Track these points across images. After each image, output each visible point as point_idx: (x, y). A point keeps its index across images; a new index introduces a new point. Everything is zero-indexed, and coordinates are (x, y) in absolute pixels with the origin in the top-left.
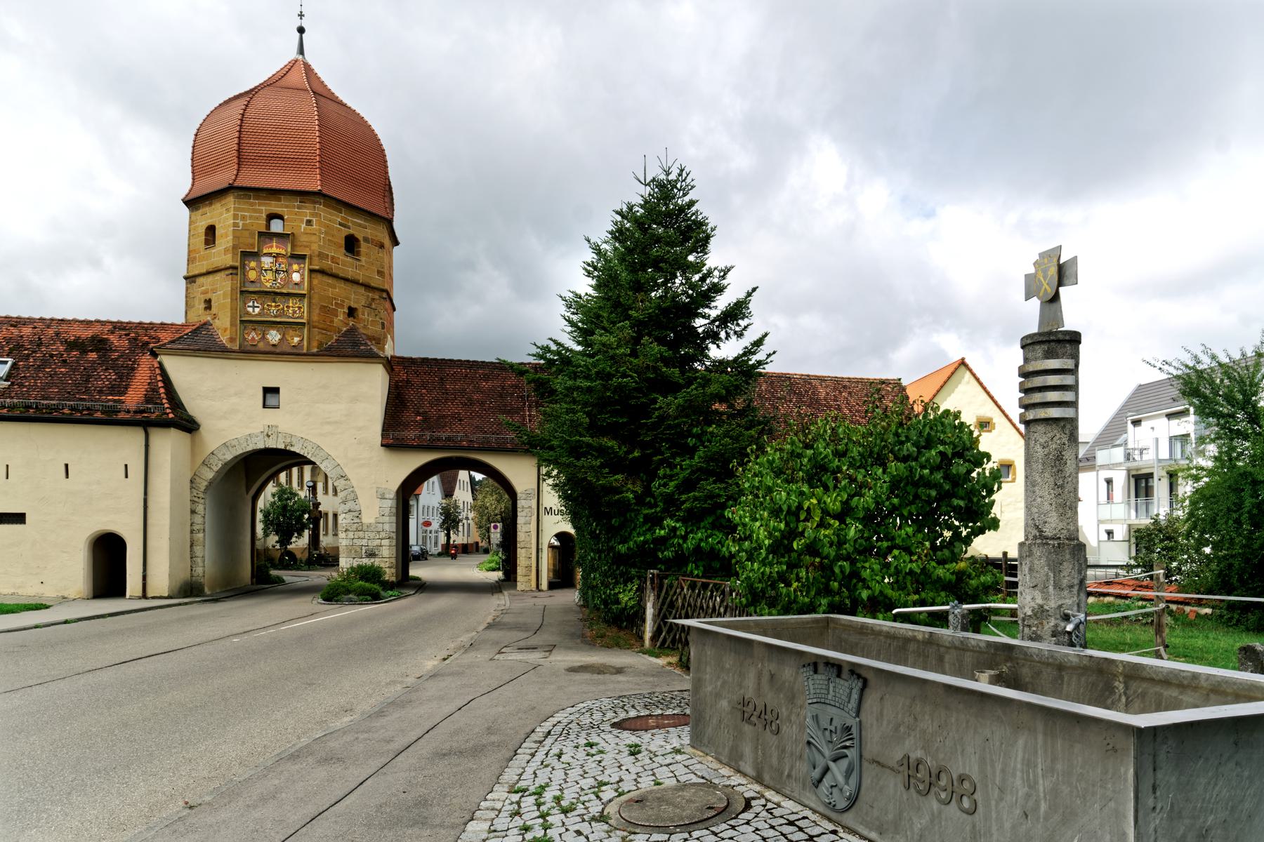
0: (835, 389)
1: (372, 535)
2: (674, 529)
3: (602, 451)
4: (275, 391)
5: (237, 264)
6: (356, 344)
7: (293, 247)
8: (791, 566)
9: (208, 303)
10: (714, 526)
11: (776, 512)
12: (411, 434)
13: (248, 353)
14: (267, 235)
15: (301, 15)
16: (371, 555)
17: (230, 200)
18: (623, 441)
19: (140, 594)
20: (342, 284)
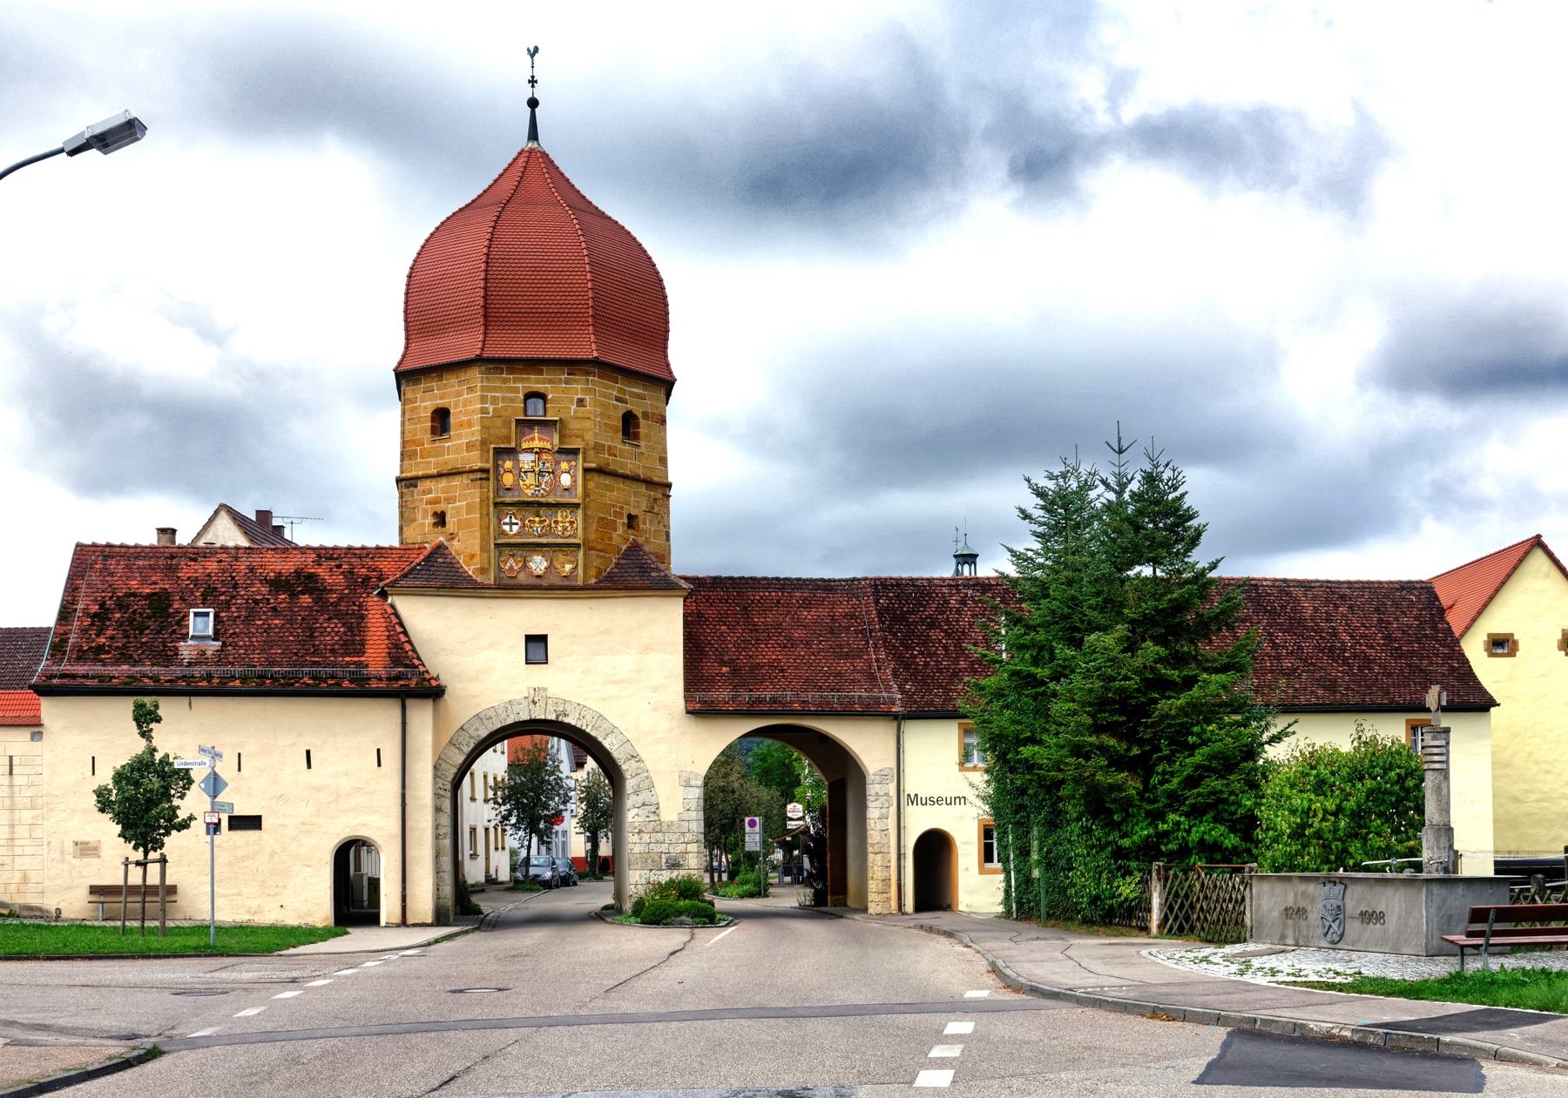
0: (1327, 601)
1: (674, 838)
2: (1178, 823)
3: (1103, 749)
4: (542, 639)
5: (489, 465)
6: (644, 570)
7: (562, 437)
8: (1304, 846)
9: (441, 519)
10: (1216, 820)
11: (1293, 812)
12: (722, 694)
13: (508, 588)
14: (525, 425)
16: (674, 865)
17: (475, 374)
18: (1120, 738)
19: (397, 919)
20: (621, 485)
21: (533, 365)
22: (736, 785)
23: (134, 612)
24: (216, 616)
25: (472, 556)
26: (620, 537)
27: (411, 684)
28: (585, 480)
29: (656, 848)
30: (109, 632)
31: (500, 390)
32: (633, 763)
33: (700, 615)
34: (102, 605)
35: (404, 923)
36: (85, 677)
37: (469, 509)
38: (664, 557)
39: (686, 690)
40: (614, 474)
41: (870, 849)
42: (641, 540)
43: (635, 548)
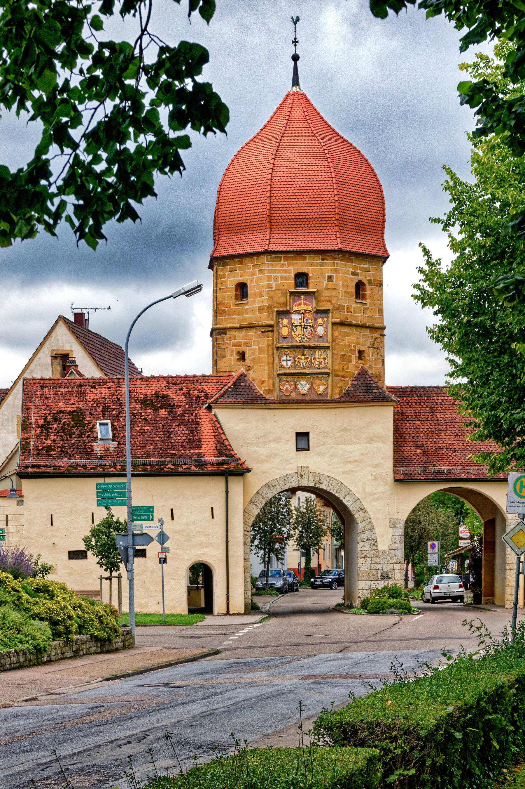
1: (386, 560)
4: (307, 434)
5: (272, 323)
6: (368, 388)
7: (318, 302)
9: (242, 356)
12: (416, 468)
13: (285, 403)
15: (295, 42)
16: (385, 577)
19: (224, 611)
21: (300, 254)
22: (422, 518)
23: (64, 423)
24: (112, 425)
25: (263, 382)
26: (354, 367)
27: (230, 468)
28: (332, 327)
29: (375, 567)
30: (52, 437)
31: (280, 271)
32: (361, 514)
33: (403, 414)
34: (45, 420)
35: (228, 613)
36: (45, 466)
37: (261, 351)
38: (381, 376)
39: (395, 466)
40: (350, 325)
41: (508, 567)
42: (366, 367)
43: (363, 373)
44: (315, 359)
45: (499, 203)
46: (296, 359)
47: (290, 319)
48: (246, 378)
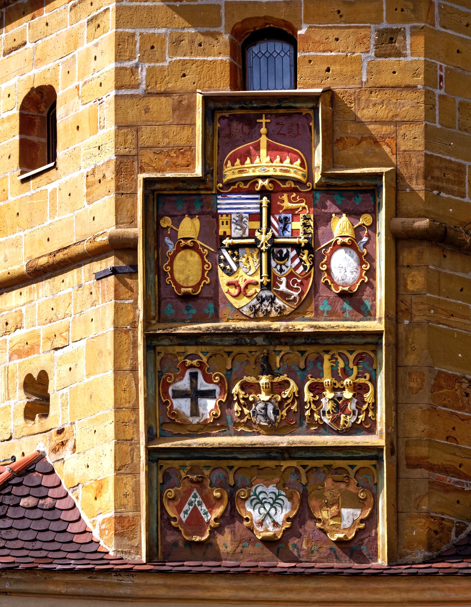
44: (317, 389)
45: (317, 524)
46: (236, 389)
47: (211, 218)
48: (47, 481)
